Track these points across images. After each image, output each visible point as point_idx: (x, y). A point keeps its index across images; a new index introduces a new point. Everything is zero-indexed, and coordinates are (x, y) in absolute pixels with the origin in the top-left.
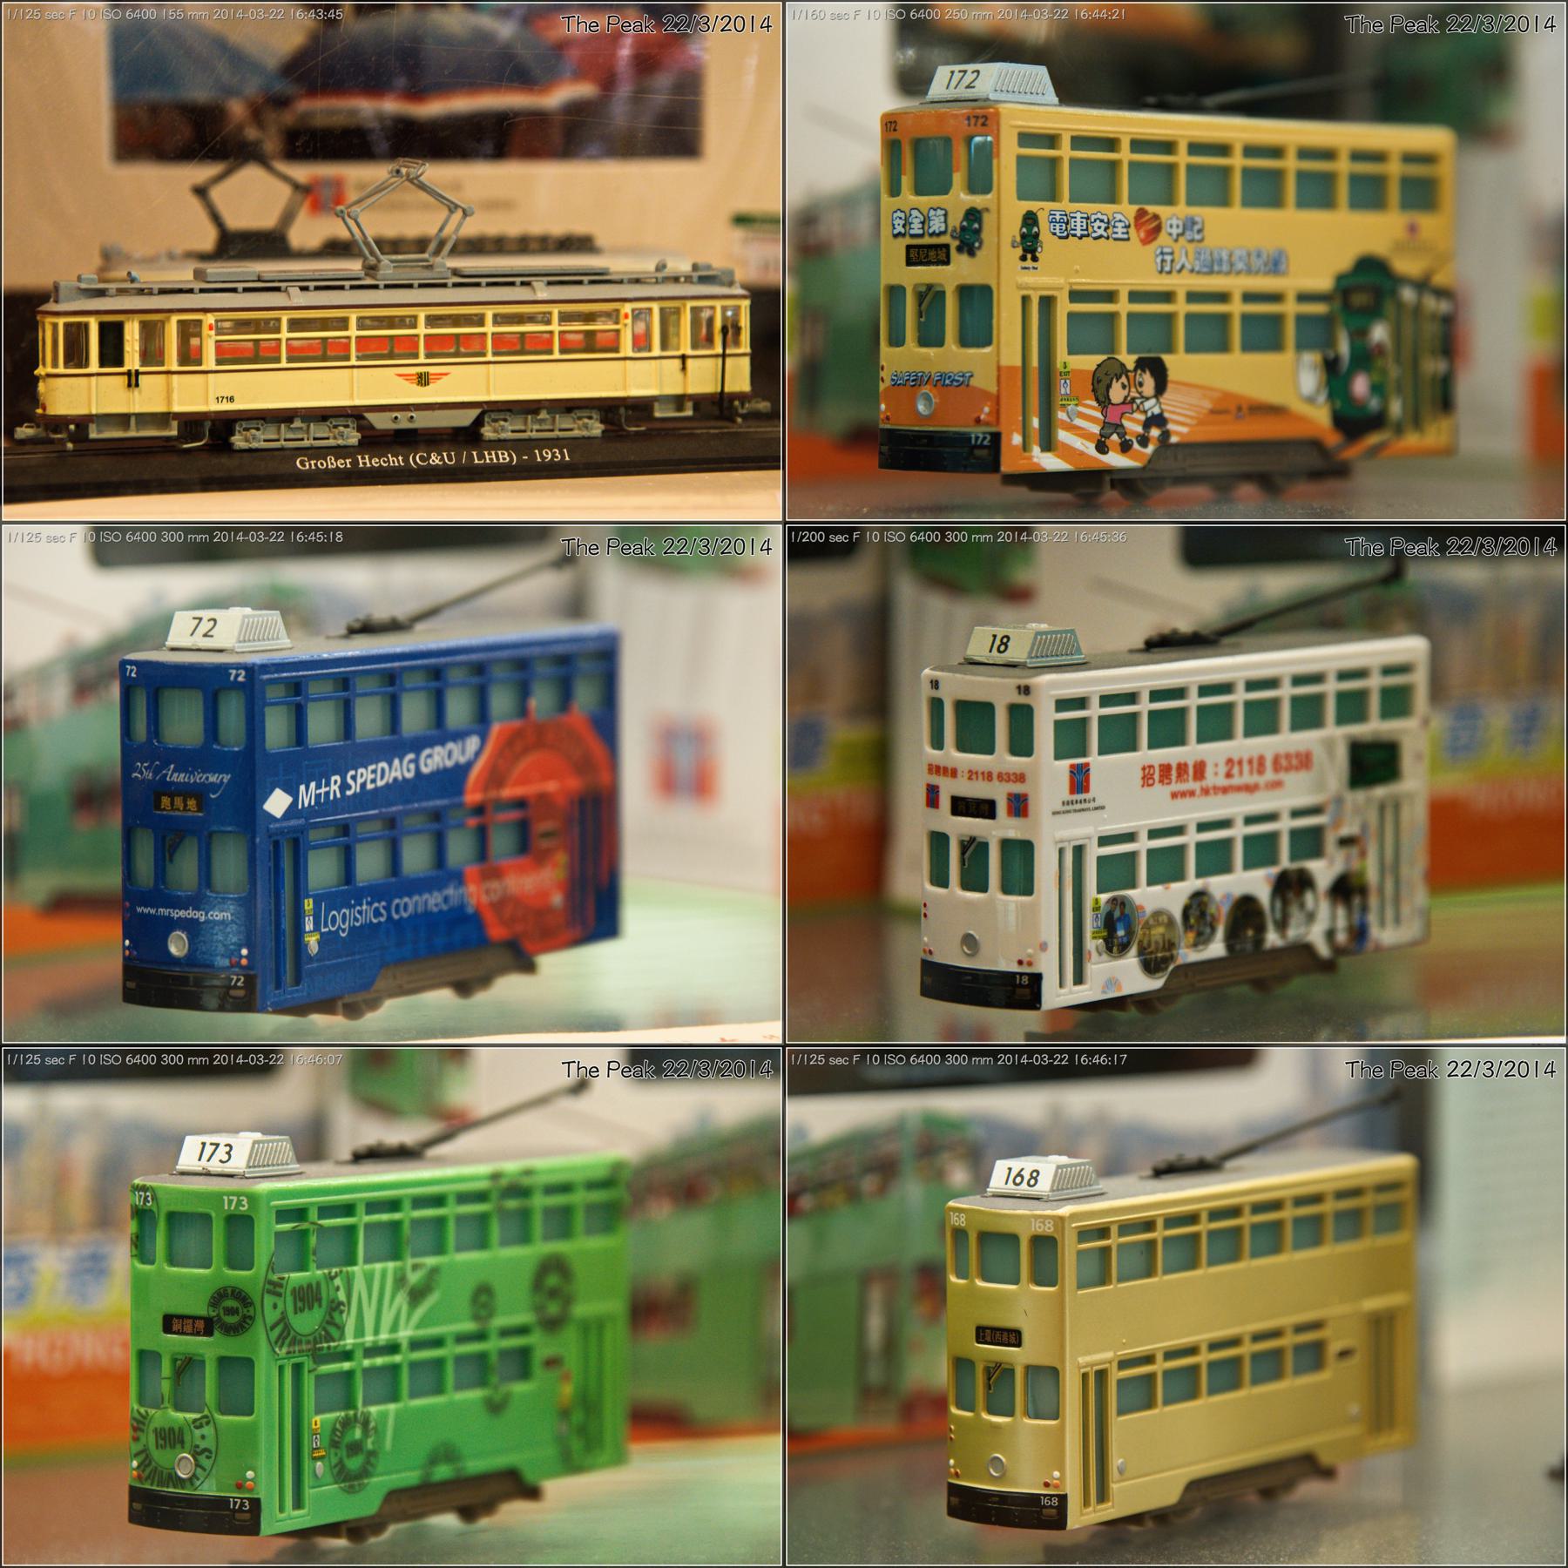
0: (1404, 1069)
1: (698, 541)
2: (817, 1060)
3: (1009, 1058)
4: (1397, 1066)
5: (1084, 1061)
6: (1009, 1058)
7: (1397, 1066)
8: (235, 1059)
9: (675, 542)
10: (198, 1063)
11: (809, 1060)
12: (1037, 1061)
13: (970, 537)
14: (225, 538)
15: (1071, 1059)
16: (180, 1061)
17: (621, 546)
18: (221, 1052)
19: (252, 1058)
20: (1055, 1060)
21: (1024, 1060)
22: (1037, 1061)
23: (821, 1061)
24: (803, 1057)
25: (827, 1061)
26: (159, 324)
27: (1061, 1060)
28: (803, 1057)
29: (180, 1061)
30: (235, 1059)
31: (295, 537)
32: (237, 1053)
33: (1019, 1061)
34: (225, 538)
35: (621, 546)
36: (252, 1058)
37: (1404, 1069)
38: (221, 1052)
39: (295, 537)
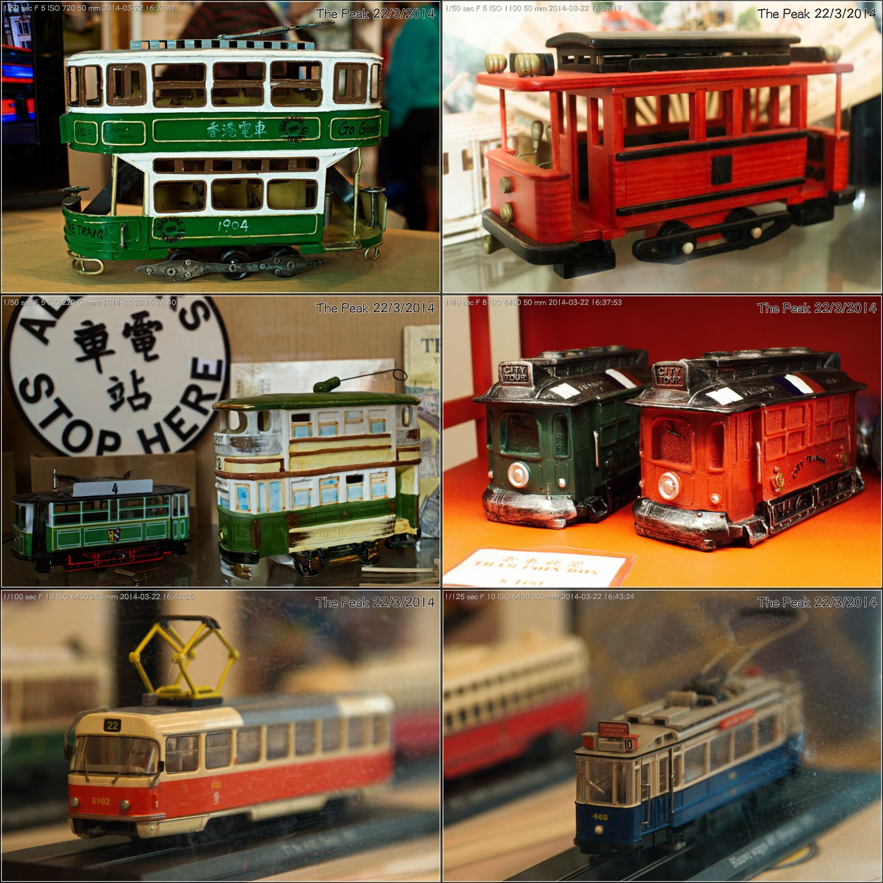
0: (791, 602)
1: (393, 304)
2: (460, 597)
3: (555, 302)
4: (787, 600)
5: (598, 303)
6: (555, 302)
7: (787, 600)
8: (561, 302)
9: (380, 305)
10: (540, 304)
11: (456, 597)
12: (142, 597)
13: (533, 303)
14: (555, 303)
15: (590, 302)
16: (530, 303)
17: (349, 308)
18: (553, 298)
19: (571, 301)
20: (581, 302)
21: (564, 303)
22: (142, 597)
23: (462, 597)
24: (452, 595)
25: (466, 598)
26: (527, 303)
27: (585, 303)
28: (452, 595)
29: (530, 303)
30: (561, 302)
31: (595, 302)
32: (562, 299)
33: (574, 597)
34: (555, 303)
35: (349, 308)
36: (571, 301)
37: (791, 602)
38: (553, 298)
39: (595, 302)
